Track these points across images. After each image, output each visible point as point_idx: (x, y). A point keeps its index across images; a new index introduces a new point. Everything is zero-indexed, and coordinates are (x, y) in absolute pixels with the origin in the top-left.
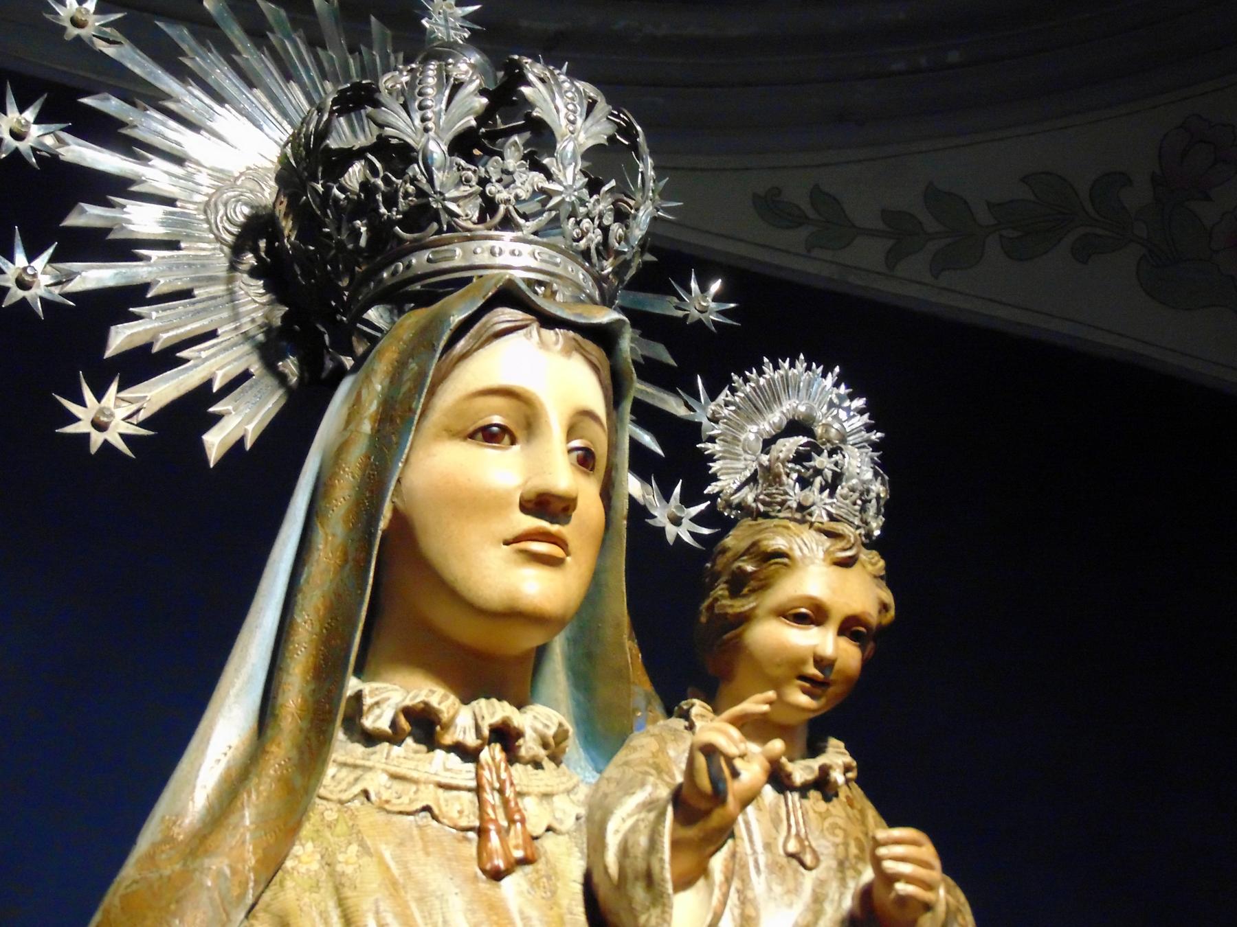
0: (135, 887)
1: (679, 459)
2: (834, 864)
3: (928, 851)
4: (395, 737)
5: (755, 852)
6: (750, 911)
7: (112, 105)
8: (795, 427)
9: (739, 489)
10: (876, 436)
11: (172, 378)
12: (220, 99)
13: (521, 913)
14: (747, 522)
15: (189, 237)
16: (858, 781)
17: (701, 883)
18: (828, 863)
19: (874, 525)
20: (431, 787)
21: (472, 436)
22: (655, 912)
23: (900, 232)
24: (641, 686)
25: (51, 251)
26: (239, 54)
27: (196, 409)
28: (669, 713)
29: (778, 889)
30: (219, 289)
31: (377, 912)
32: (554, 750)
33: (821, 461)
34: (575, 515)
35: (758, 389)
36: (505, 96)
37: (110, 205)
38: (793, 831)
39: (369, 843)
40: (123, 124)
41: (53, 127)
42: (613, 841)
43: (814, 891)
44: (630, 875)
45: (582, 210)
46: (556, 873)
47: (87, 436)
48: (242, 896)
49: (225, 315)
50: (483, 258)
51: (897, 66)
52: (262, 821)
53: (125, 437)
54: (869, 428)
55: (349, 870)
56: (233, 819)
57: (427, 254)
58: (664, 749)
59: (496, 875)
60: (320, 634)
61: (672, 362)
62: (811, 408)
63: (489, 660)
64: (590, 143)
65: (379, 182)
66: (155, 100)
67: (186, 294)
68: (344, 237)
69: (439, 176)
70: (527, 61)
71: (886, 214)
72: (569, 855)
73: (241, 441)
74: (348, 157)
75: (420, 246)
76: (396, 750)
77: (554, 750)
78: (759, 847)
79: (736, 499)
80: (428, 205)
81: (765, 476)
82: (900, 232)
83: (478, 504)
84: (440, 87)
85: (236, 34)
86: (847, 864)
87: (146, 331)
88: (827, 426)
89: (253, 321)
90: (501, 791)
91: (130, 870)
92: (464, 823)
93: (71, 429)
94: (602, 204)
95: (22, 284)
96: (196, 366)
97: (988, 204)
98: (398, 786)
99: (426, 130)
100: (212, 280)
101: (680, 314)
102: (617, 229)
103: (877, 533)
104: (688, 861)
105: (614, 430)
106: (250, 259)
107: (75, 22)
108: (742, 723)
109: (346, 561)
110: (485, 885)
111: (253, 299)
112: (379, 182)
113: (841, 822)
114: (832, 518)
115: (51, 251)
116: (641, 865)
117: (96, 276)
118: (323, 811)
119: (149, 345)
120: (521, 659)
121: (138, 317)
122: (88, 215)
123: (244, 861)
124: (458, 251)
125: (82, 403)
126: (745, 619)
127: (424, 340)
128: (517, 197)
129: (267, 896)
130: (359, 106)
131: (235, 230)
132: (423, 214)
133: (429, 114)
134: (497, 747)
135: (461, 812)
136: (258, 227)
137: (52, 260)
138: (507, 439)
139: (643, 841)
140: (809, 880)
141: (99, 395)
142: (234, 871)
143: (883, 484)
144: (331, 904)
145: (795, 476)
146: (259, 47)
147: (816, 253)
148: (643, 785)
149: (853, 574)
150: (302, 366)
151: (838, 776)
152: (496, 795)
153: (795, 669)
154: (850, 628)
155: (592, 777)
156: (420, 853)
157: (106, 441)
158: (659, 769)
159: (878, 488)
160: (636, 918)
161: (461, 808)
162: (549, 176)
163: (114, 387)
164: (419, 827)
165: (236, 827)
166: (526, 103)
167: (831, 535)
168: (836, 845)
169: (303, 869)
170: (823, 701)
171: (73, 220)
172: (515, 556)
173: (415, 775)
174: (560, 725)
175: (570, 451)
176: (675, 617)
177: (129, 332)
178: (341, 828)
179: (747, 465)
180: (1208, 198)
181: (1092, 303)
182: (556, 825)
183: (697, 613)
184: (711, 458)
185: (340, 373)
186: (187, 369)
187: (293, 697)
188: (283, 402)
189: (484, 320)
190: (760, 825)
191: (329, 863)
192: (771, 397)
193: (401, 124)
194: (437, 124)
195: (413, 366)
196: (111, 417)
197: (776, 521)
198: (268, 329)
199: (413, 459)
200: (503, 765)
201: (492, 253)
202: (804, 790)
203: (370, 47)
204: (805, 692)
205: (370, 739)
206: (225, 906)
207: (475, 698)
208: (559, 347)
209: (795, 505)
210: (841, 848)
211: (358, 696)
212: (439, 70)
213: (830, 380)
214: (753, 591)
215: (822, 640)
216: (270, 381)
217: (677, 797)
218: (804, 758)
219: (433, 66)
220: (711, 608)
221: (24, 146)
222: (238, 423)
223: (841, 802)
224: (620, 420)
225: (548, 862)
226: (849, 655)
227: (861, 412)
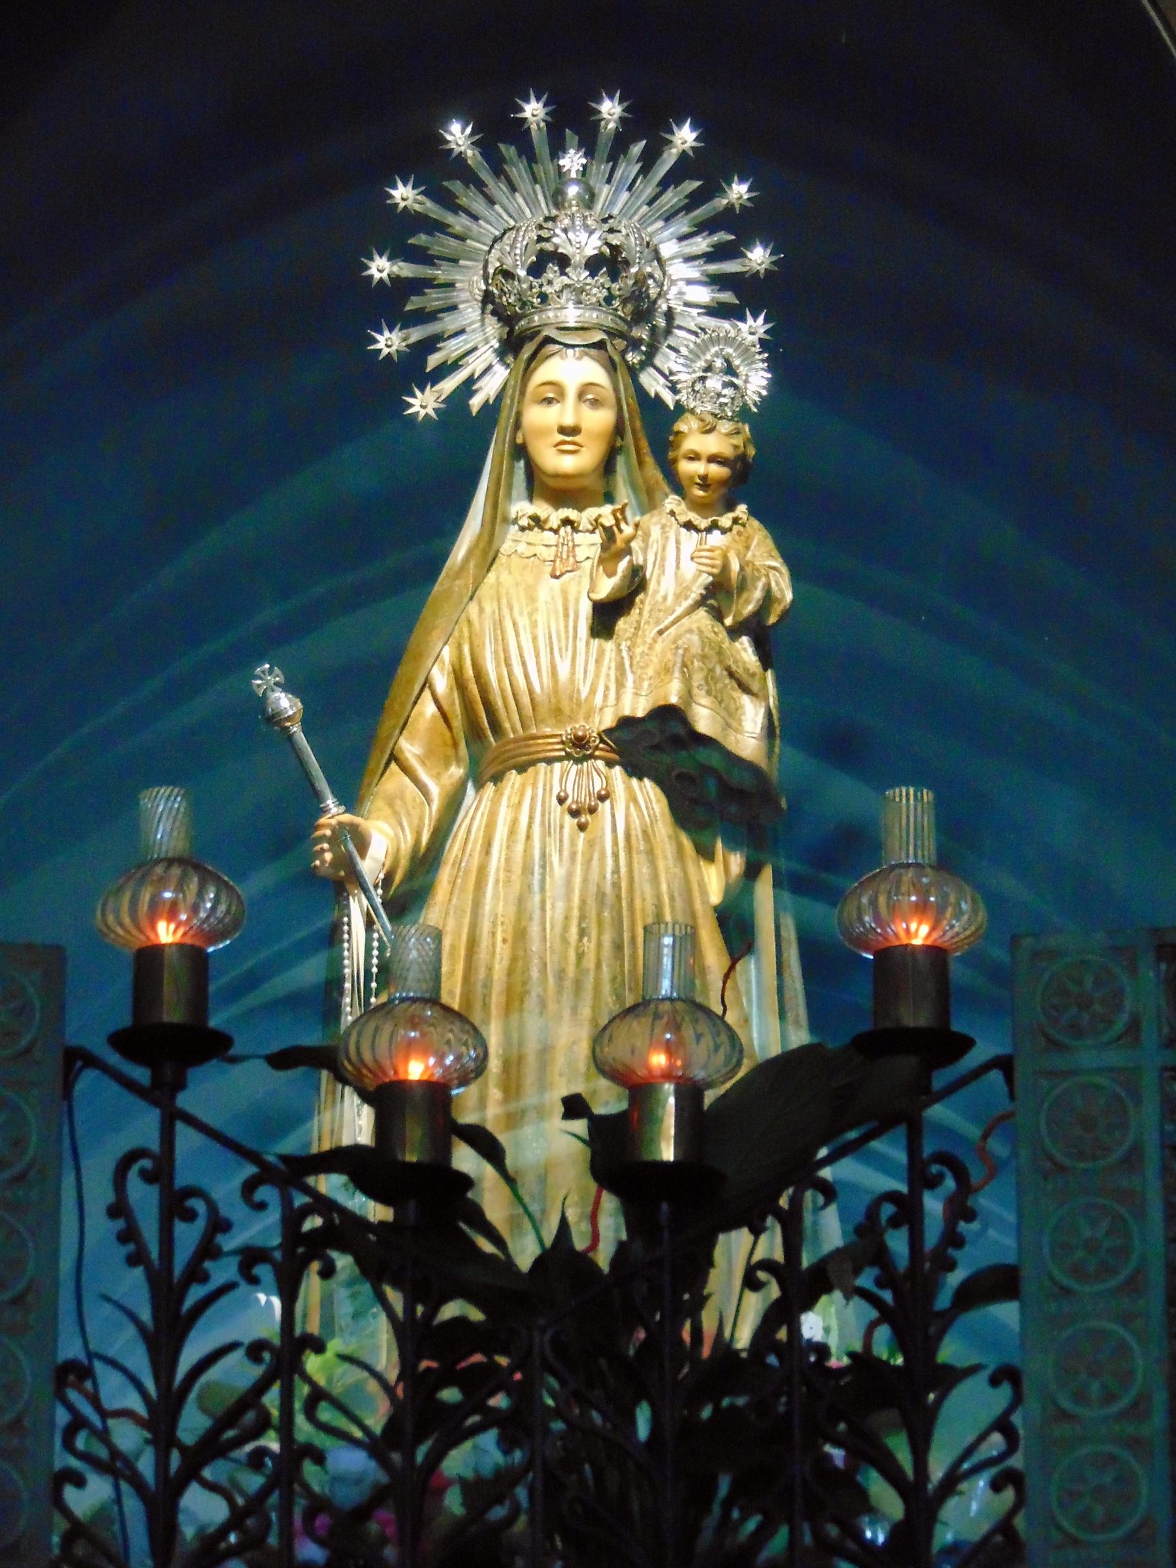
4: (530, 528)
27: (468, 387)
83: (543, 432)
85: (486, 176)
93: (410, 411)
124: (536, 318)
146: (456, 213)
163: (429, 387)
222: (488, 389)
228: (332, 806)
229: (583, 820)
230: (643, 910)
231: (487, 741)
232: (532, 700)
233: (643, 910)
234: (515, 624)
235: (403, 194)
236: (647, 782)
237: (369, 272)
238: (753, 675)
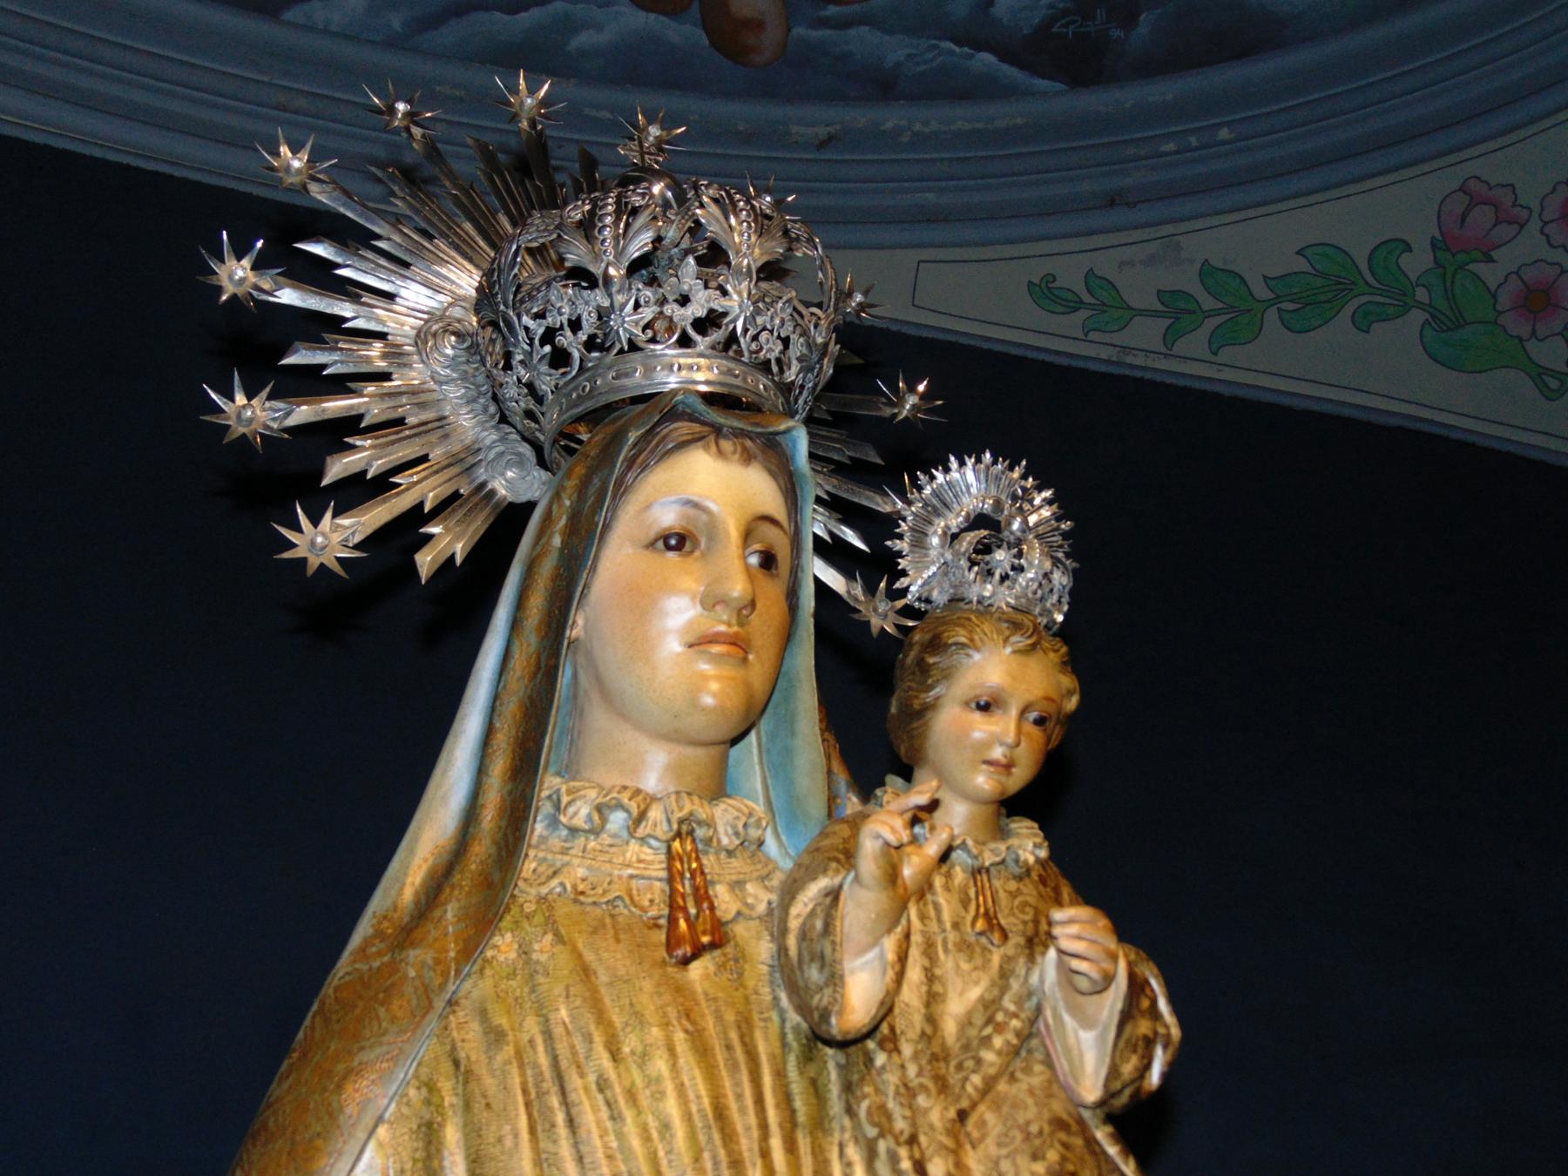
0: (347, 978)
2: (1022, 941)
6: (938, 988)
10: (1066, 526)
18: (1016, 940)
25: (268, 390)
39: (563, 932)
42: (794, 924)
43: (1001, 967)
46: (744, 957)
47: (304, 560)
56: (437, 913)
72: (759, 938)
84: (618, 214)
86: (1036, 940)
96: (407, 489)
109: (539, 668)
113: (1030, 900)
115: (268, 390)
119: (365, 472)
121: (353, 447)
135: (651, 901)
139: (819, 924)
147: (1093, 336)
156: (611, 941)
163: (328, 515)
168: (1025, 923)
169: (502, 959)
178: (538, 919)
180: (1491, 260)
191: (524, 951)
196: (327, 539)
223: (1032, 882)
225: (736, 945)
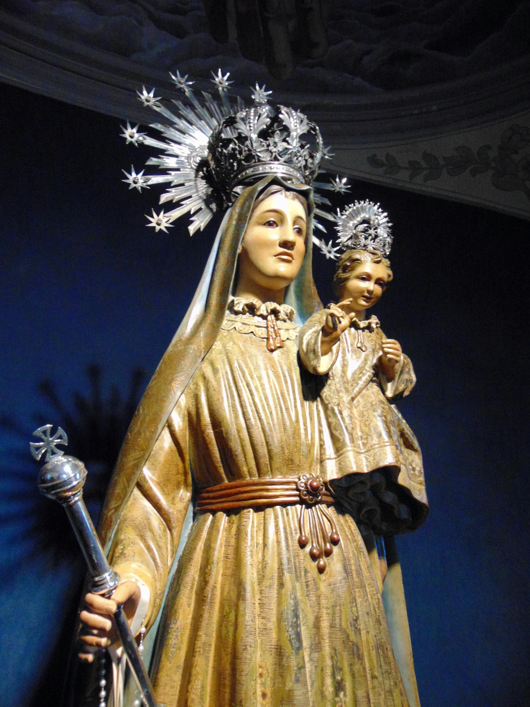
1: (330, 234)
3: (398, 346)
4: (243, 313)
5: (348, 346)
6: (346, 363)
7: (159, 127)
8: (364, 221)
9: (347, 241)
10: (390, 225)
11: (179, 210)
12: (191, 124)
13: (279, 361)
14: (349, 251)
15: (184, 167)
16: (381, 327)
17: (330, 353)
18: (370, 350)
19: (387, 251)
20: (254, 326)
21: (265, 224)
22: (316, 361)
23: (415, 167)
24: (317, 300)
26: (196, 109)
28: (325, 307)
29: (354, 357)
30: (192, 183)
31: (237, 360)
32: (290, 317)
33: (372, 231)
34: (295, 247)
35: (353, 210)
36: (275, 119)
37: (159, 158)
38: (360, 341)
39: (235, 341)
40: (162, 133)
41: (142, 134)
44: (309, 351)
45: (299, 154)
47: (155, 227)
48: (200, 355)
49: (194, 191)
50: (268, 170)
51: (416, 112)
52: (206, 336)
53: (166, 227)
54: (388, 222)
55: (230, 348)
56: (198, 335)
57: (251, 169)
58: (320, 317)
59: (272, 351)
60: (221, 283)
61: (330, 204)
62: (370, 216)
63: (272, 290)
64: (301, 133)
65: (237, 147)
66: (171, 124)
67: (182, 185)
68: (227, 165)
69: (255, 145)
70: (282, 107)
71: (410, 162)
72: (294, 346)
73: (199, 229)
74: (230, 141)
75: (249, 167)
76: (244, 316)
77: (290, 317)
78: (349, 345)
79: (346, 244)
80: (251, 154)
81: (355, 237)
82: (414, 168)
83: (266, 244)
84: (255, 116)
85: (196, 103)
87: (171, 196)
88: (374, 221)
89: (202, 193)
90: (274, 328)
91: (170, 348)
92: (263, 336)
94: (305, 152)
95: (135, 183)
97: (444, 157)
98: (244, 326)
99: (251, 130)
100: (190, 180)
101: (333, 189)
102: (310, 161)
103: (388, 253)
104: (326, 347)
105: (308, 223)
106: (201, 173)
107: (147, 101)
108: (343, 307)
110: (268, 353)
111: (202, 186)
112: (237, 147)
113: (374, 339)
114: (374, 249)
116: (312, 348)
117: (156, 179)
118: (223, 333)
119: (172, 200)
120: (279, 291)
122: (153, 161)
123: (201, 346)
124: (261, 168)
125: (153, 217)
126: (347, 279)
127: (250, 196)
128: (278, 151)
129: (207, 356)
130: (232, 124)
131: (197, 165)
132: (250, 157)
133: (252, 125)
134: (273, 316)
136: (203, 164)
137: (144, 175)
138: (275, 225)
139: (313, 341)
140: (363, 354)
141: (158, 215)
142: (198, 349)
143: (391, 238)
144: (225, 358)
145: (363, 236)
148: (314, 326)
149: (380, 266)
150: (217, 205)
151: (374, 326)
152: (272, 329)
153: (361, 294)
154: (378, 282)
155: (301, 325)
156: (250, 345)
157: (160, 229)
158: (320, 322)
159: (389, 240)
160: (310, 362)
161: (262, 332)
162: (288, 144)
163: (162, 213)
164: (250, 337)
165: (199, 337)
166: (282, 121)
167: (373, 254)
168: (372, 345)
170: (370, 304)
171: (149, 163)
172: (278, 260)
173: (249, 323)
174: (292, 310)
175: (294, 229)
176: (327, 279)
177: (166, 196)
178: (228, 337)
179: (349, 234)
181: (476, 190)
182: (289, 338)
183: (333, 278)
184: (338, 232)
185: (228, 207)
186: (183, 208)
187: (214, 301)
188: (212, 217)
189: (268, 189)
190: (349, 337)
191: (224, 347)
192: (357, 213)
193: (243, 128)
194: (254, 128)
195: (247, 204)
196: (161, 221)
197: (357, 250)
198: (208, 196)
199: (248, 232)
200: (274, 321)
201: (271, 168)
202: (363, 329)
203: (237, 106)
204: (364, 301)
205: (237, 313)
206: (196, 358)
207: (267, 302)
208: (291, 197)
209: (363, 245)
210: (374, 346)
211: (233, 301)
212: (255, 111)
213: (376, 207)
214: (349, 271)
215: (370, 285)
216: (208, 211)
217: (323, 329)
218: (364, 320)
219: (252, 111)
220: (337, 276)
221: (133, 140)
222: (198, 223)
224: (310, 219)
225: (287, 348)
226: (378, 290)
227: (385, 217)
228: (108, 578)
229: (322, 563)
230: (368, 642)
231: (218, 477)
232: (269, 451)
233: (368, 642)
234: (248, 385)
235: (147, 96)
236: (349, 519)
237: (124, 135)
238: (188, 374)
